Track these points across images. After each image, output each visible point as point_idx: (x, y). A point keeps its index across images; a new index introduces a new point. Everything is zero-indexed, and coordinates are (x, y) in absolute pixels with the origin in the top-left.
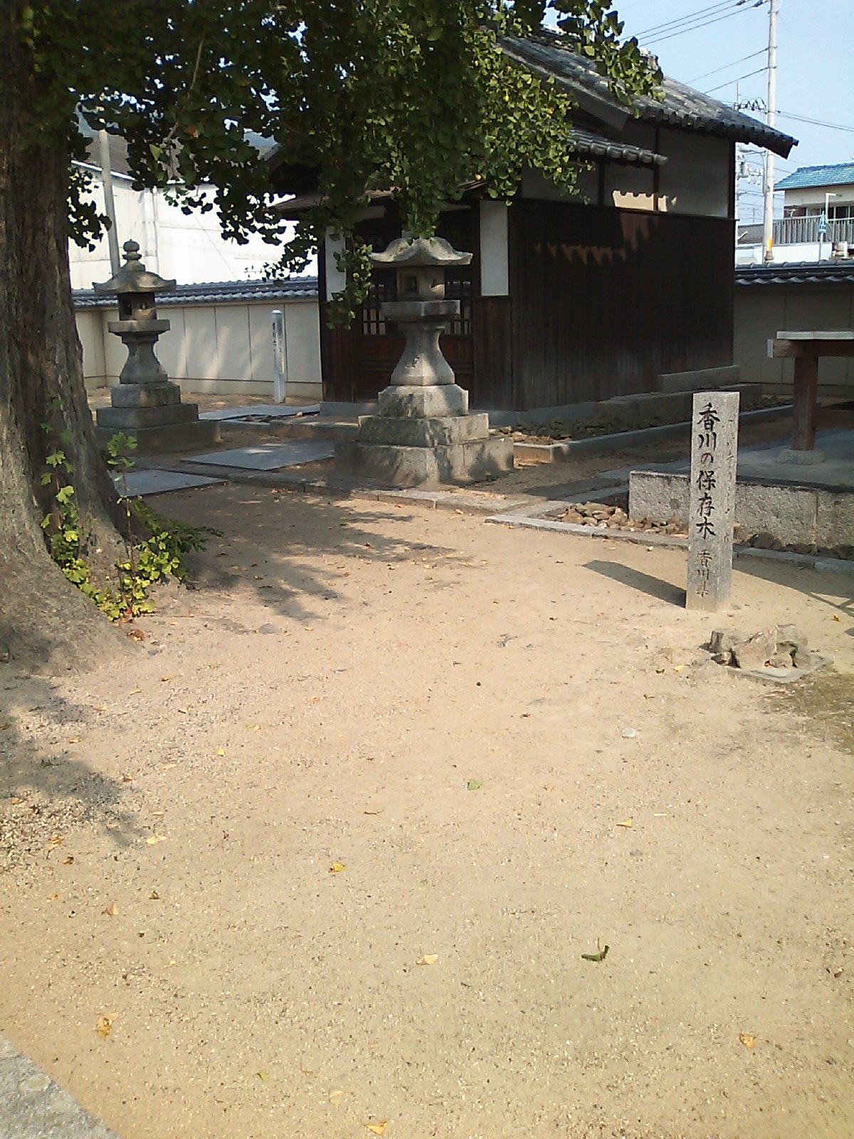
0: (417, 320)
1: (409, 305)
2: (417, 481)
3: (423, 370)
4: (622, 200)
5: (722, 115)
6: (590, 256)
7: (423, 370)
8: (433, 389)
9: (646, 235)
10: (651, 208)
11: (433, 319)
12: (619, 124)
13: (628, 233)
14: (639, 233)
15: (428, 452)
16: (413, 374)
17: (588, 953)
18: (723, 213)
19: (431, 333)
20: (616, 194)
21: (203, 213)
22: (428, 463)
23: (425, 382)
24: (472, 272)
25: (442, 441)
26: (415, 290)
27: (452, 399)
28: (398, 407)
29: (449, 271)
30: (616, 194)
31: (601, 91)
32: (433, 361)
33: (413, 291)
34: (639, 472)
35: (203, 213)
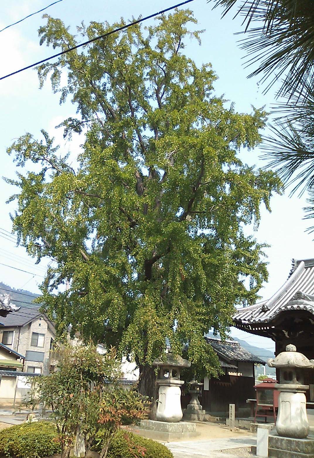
0: (194, 393)
1: (194, 391)
2: (194, 420)
3: (195, 402)
4: (230, 374)
5: (251, 358)
6: (224, 385)
7: (195, 402)
8: (196, 405)
9: (235, 381)
10: (236, 375)
11: (197, 393)
12: (229, 361)
13: (232, 380)
14: (234, 381)
15: (196, 415)
16: (193, 403)
17: (193, 23)
18: (252, 376)
19: (196, 397)
20: (229, 373)
21: (267, 282)
22: (196, 416)
23: (195, 404)
24: (203, 386)
25: (198, 414)
26: (194, 389)
27: (200, 407)
28: (191, 407)
29: (200, 386)
30: (229, 373)
31: (226, 355)
32: (196, 400)
33: (194, 389)
34: (219, 352)
35: (267, 282)
